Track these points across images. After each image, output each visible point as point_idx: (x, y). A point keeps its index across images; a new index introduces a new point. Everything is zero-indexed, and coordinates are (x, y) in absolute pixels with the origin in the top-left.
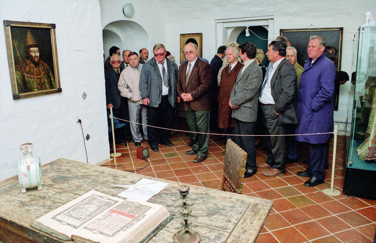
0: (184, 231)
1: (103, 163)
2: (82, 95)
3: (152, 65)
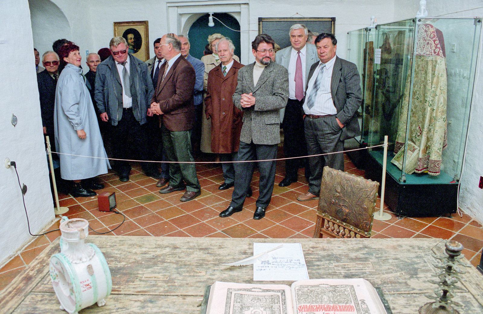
0: (438, 305)
1: (48, 228)
2: (10, 118)
3: (109, 67)
